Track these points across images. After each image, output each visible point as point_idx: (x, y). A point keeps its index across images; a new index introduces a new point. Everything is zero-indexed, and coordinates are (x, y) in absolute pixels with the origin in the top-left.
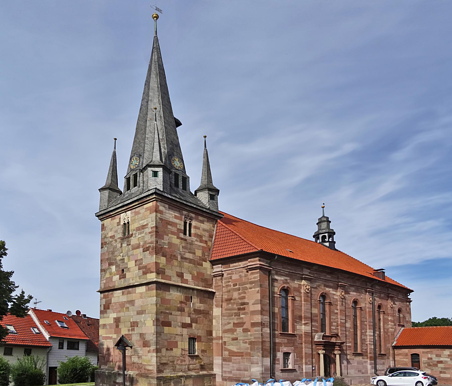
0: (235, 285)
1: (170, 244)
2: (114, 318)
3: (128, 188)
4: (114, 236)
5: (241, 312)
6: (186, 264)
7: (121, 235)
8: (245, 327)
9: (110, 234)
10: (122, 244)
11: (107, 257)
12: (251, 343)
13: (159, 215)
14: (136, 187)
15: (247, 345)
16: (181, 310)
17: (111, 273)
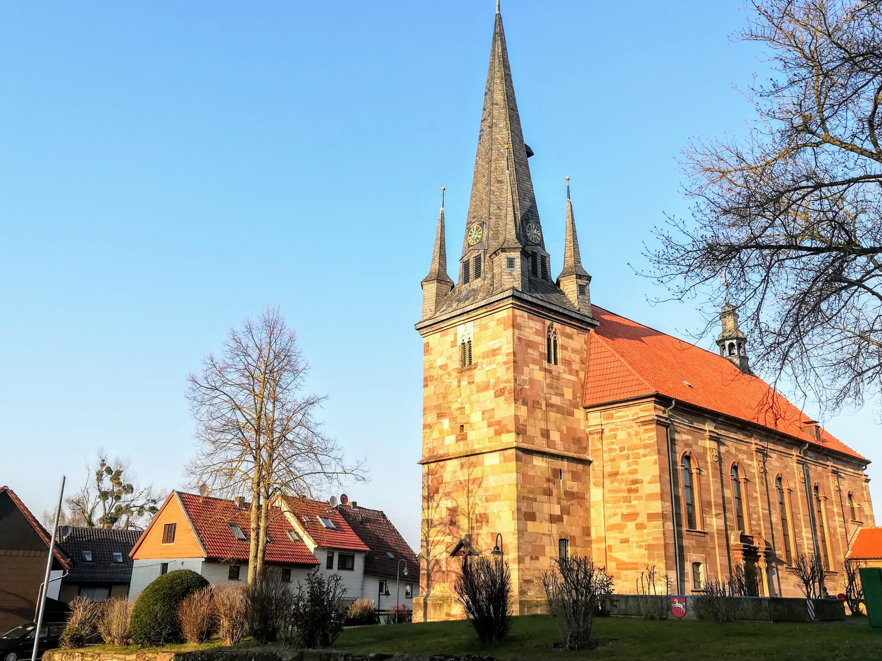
0: (622, 449)
1: (532, 381)
2: (448, 509)
3: (466, 280)
4: (446, 365)
5: (633, 495)
6: (553, 415)
7: (457, 364)
8: (640, 520)
9: (439, 362)
10: (459, 382)
11: (434, 403)
12: (649, 547)
13: (516, 331)
14: (479, 279)
15: (643, 551)
16: (549, 493)
17: (441, 432)
